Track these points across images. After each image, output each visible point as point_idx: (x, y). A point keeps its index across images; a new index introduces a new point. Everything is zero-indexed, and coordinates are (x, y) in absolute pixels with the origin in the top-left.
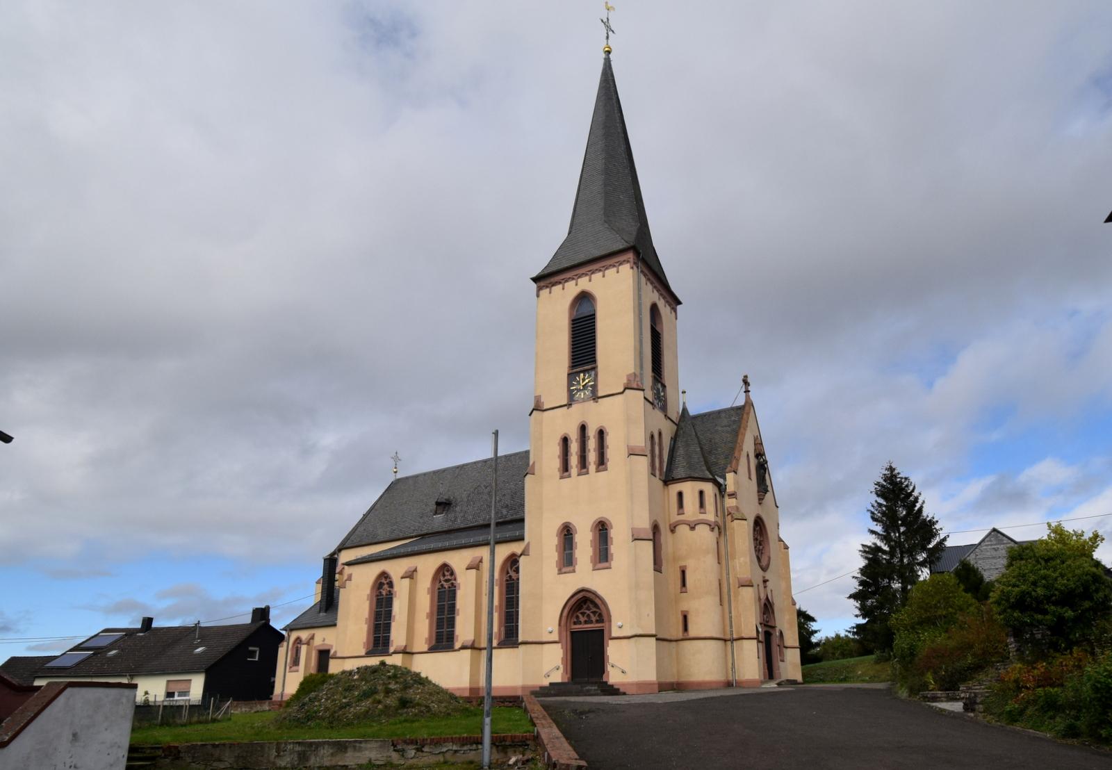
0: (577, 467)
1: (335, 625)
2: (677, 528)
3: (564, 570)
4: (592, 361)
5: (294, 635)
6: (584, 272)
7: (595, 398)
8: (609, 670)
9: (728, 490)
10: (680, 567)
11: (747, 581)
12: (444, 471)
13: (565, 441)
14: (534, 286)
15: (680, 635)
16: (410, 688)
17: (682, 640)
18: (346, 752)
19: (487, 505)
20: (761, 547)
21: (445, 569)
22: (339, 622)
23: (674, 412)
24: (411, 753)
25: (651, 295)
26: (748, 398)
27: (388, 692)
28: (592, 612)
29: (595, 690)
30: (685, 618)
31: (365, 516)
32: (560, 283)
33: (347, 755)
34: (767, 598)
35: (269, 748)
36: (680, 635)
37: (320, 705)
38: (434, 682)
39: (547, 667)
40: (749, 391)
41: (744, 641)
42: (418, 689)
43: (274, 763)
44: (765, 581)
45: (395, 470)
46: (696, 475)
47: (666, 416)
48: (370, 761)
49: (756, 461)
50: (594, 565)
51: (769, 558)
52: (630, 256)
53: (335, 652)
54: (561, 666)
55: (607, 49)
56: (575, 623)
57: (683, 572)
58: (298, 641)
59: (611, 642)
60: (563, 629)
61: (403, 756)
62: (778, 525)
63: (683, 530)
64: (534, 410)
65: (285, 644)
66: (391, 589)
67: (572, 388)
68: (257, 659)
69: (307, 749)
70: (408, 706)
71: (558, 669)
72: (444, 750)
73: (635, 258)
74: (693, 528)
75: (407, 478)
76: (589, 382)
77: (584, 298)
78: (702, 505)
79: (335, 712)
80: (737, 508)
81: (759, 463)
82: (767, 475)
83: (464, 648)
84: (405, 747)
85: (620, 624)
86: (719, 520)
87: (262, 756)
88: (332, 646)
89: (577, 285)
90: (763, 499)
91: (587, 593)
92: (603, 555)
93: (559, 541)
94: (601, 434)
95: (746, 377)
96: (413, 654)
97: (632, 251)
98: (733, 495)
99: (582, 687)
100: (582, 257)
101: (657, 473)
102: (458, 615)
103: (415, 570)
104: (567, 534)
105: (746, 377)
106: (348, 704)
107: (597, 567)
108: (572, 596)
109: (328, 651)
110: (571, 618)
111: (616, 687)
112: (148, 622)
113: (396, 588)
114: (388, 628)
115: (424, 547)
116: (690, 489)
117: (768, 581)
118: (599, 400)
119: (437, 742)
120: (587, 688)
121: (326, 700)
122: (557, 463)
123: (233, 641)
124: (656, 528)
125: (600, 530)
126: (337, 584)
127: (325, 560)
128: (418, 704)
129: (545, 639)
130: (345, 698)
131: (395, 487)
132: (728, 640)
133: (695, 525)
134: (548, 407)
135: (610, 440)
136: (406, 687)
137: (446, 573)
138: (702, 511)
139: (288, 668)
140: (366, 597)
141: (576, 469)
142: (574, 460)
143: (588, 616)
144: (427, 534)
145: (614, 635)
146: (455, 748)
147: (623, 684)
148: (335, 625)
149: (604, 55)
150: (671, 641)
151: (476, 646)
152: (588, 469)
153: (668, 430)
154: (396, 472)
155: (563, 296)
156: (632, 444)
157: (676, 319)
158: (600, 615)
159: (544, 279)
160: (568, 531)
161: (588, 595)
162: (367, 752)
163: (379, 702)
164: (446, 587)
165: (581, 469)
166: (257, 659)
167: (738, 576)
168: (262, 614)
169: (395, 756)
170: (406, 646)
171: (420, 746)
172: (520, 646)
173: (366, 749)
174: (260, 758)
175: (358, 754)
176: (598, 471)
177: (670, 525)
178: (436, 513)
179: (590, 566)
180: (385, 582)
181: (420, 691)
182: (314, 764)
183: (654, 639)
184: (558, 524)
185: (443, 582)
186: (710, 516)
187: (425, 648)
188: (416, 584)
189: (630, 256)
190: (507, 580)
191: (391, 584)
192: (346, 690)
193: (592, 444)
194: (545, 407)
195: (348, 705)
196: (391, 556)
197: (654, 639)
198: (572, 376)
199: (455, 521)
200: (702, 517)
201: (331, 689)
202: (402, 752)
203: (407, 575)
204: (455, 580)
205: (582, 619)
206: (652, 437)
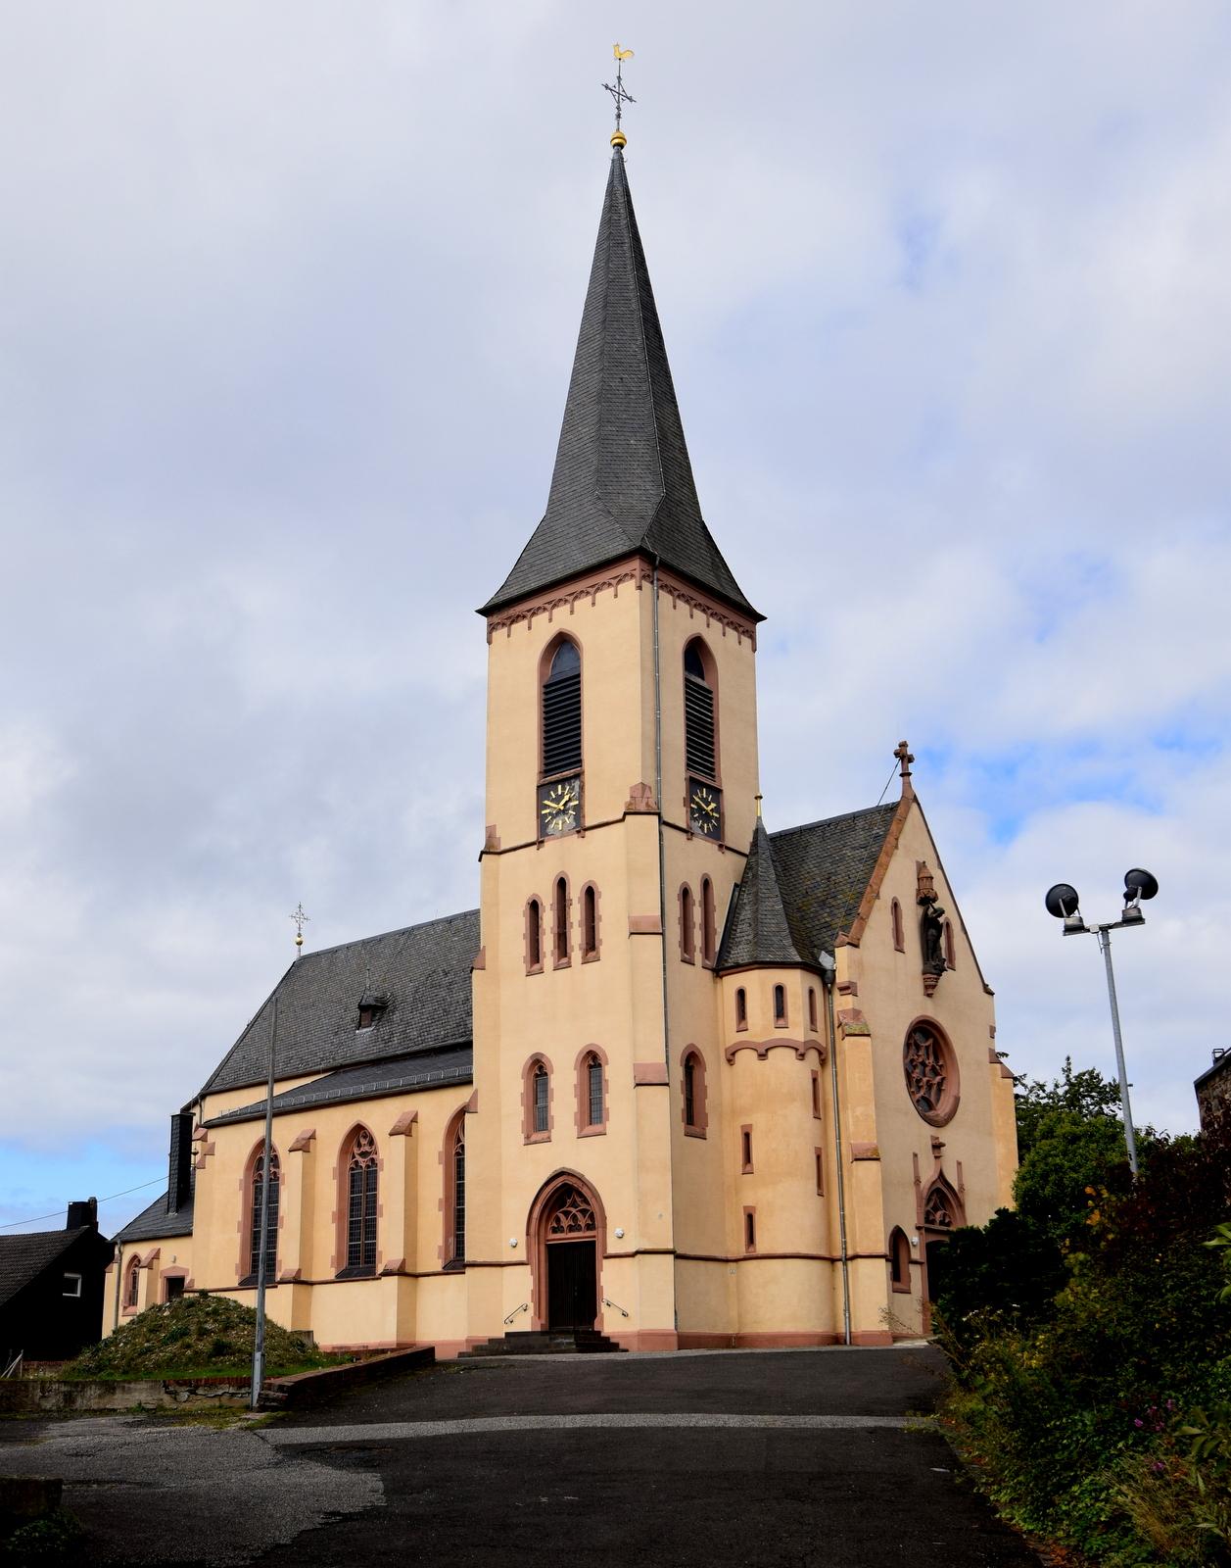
0: (553, 954)
1: (189, 1234)
2: (738, 1055)
3: (534, 1137)
4: (575, 763)
5: (129, 1251)
7: (581, 830)
9: (838, 980)
10: (742, 1127)
11: (867, 1150)
12: (380, 940)
13: (534, 907)
15: (742, 1252)
16: (233, 1328)
17: (745, 1259)
18: (113, 1394)
19: (445, 1010)
20: (938, 1078)
21: (359, 1134)
22: (196, 1230)
23: (739, 835)
24: (185, 1396)
25: (685, 621)
26: (907, 786)
27: (203, 1333)
28: (580, 1211)
29: (567, 1343)
30: (750, 1218)
31: (251, 1026)
32: (524, 617)
33: (116, 1397)
35: (33, 1387)
36: (739, 1248)
37: (117, 1351)
38: (279, 1325)
39: (509, 1306)
40: (910, 774)
41: (859, 1260)
42: (245, 1329)
43: (39, 1405)
44: (937, 1147)
45: (298, 939)
46: (770, 958)
47: (721, 846)
48: (140, 1404)
49: (921, 910)
50: (581, 1128)
51: (957, 1100)
52: (635, 565)
53: (192, 1281)
54: (531, 1306)
55: (617, 141)
56: (555, 1231)
57: (747, 1136)
58: (136, 1262)
59: (605, 1262)
60: (534, 1241)
61: (175, 1399)
62: (993, 1030)
63: (746, 1058)
64: (482, 853)
65: (115, 1266)
67: (543, 812)
68: (78, 1295)
69: (73, 1389)
70: (225, 1352)
72: (220, 1392)
73: (646, 566)
74: (763, 1056)
75: (318, 954)
76: (570, 800)
77: (563, 643)
78: (780, 1012)
79: (132, 1359)
80: (856, 1014)
81: (925, 916)
82: (943, 941)
83: (387, 1273)
84: (178, 1388)
85: (619, 1231)
86: (820, 1038)
87: (27, 1396)
88: (187, 1270)
89: (550, 620)
90: (934, 987)
91: (570, 1178)
92: (593, 1112)
93: (526, 1088)
94: (590, 893)
95: (903, 745)
96: (312, 1284)
98: (846, 989)
99: (551, 1339)
100: (560, 571)
101: (698, 957)
102: (382, 1216)
103: (313, 1137)
104: (538, 1071)
105: (903, 745)
106: (149, 1350)
107: (585, 1132)
108: (547, 1184)
109: (181, 1280)
110: (547, 1221)
111: (612, 1340)
113: (284, 1169)
114: (371, 1229)
115: (338, 1092)
116: (758, 984)
118: (587, 833)
119: (211, 1384)
120: (559, 1341)
121: (126, 1344)
122: (522, 948)
123: (39, 1260)
125: (537, 1076)
128: (240, 1351)
129: (505, 1260)
130: (148, 1341)
131: (302, 971)
132: (835, 1260)
133: (767, 1050)
134: (508, 847)
135: (603, 906)
136: (227, 1327)
137: (363, 1142)
139: (121, 1308)
142: (548, 942)
144: (342, 1067)
145: (611, 1251)
146: (232, 1390)
147: (625, 1336)
148: (189, 1234)
149: (611, 152)
150: (727, 1261)
151: (408, 1270)
152: (570, 958)
153: (724, 871)
154: (300, 943)
155: (534, 634)
156: (637, 913)
157: (754, 650)
158: (592, 1217)
159: (500, 611)
160: (541, 1068)
161: (571, 1181)
162: (137, 1394)
163: (188, 1346)
164: (364, 1165)
165: (531, 966)
166: (78, 1295)
167: (852, 1142)
168: (83, 1213)
169: (166, 1398)
170: (300, 1270)
171: (193, 1387)
172: (468, 1271)
173: (136, 1390)
174: (25, 1399)
175: (127, 1396)
177: (726, 1050)
178: (359, 1026)
179: (574, 1130)
181: (246, 1332)
182: (81, 1406)
183: (672, 1256)
184: (523, 1058)
185: (358, 1158)
186: (797, 1028)
187: (331, 1274)
188: (315, 1160)
190: (352, 1169)
191: (275, 1160)
192: (151, 1331)
193: (576, 913)
194: (503, 847)
195: (150, 1351)
196: (307, 1105)
197: (672, 1256)
198: (543, 790)
199: (390, 1040)
200: (743, 1037)
201: (133, 1329)
202: (174, 1395)
203: (299, 1146)
205: (565, 1222)
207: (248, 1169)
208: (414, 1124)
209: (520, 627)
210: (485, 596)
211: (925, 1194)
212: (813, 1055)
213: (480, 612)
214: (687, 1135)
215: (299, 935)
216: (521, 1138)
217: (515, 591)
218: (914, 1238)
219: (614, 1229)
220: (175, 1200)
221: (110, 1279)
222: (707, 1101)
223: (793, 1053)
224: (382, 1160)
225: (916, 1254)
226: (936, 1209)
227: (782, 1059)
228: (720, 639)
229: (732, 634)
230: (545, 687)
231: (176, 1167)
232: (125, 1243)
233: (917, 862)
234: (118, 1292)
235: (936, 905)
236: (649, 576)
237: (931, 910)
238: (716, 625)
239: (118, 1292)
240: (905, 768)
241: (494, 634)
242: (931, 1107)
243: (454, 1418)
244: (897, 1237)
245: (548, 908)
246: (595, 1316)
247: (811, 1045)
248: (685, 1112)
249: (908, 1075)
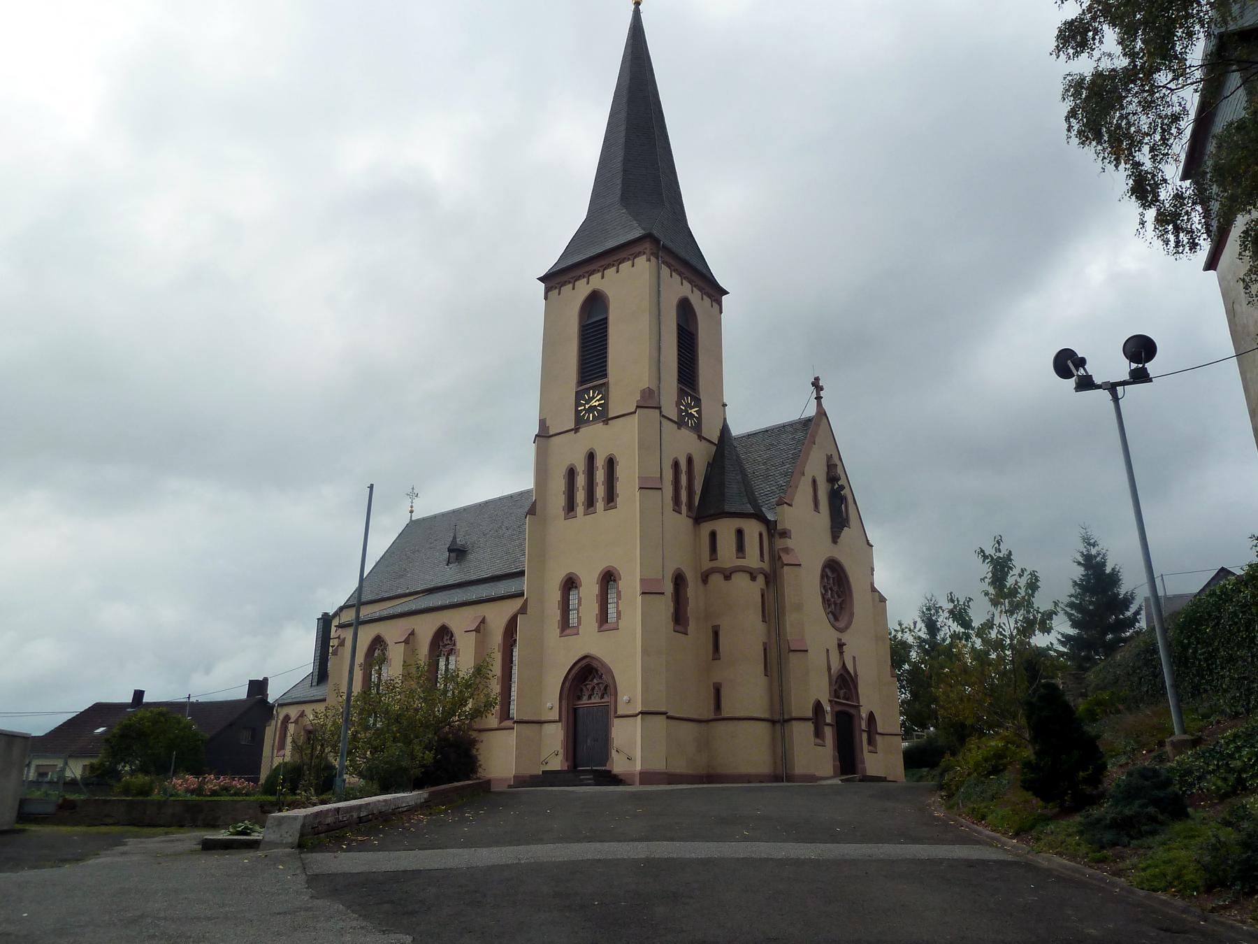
5: (283, 713)
6: (581, 274)
9: (778, 528)
13: (571, 473)
15: (712, 716)
25: (677, 288)
26: (819, 404)
44: (841, 646)
49: (829, 486)
57: (716, 634)
59: (616, 722)
63: (716, 579)
65: (273, 723)
67: (579, 409)
78: (740, 548)
94: (611, 463)
95: (817, 379)
97: (648, 240)
101: (684, 508)
105: (817, 379)
112: (139, 694)
124: (679, 580)
133: (731, 574)
135: (620, 471)
138: (740, 555)
139: (276, 751)
142: (580, 496)
145: (620, 712)
157: (721, 312)
165: (568, 513)
168: (258, 687)
186: (753, 559)
189: (647, 246)
193: (600, 476)
194: (551, 433)
197: (665, 716)
198: (579, 396)
204: (454, 645)
211: (834, 678)
212: (761, 579)
213: (541, 279)
214: (675, 631)
215: (412, 507)
216: (558, 631)
218: (828, 708)
219: (623, 697)
220: (317, 677)
222: (688, 608)
223: (748, 575)
225: (829, 719)
226: (841, 688)
227: (741, 580)
228: (700, 303)
229: (707, 300)
230: (583, 326)
231: (318, 654)
232: (281, 705)
233: (827, 455)
234: (275, 735)
235: (840, 483)
236: (655, 254)
237: (836, 486)
238: (697, 293)
239: (275, 735)
240: (818, 393)
241: (549, 293)
242: (836, 619)
243: (511, 843)
244: (818, 707)
246: (608, 759)
247: (762, 571)
248: (674, 616)
249: (823, 596)
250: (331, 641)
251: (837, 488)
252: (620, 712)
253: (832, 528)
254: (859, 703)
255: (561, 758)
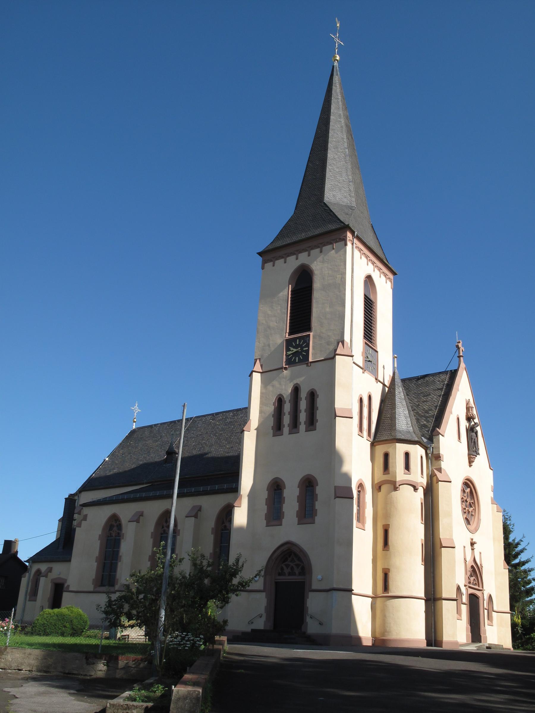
0: (305, 423)
5: (36, 567)
8: (307, 621)
14: (260, 259)
34: (475, 560)
44: (472, 544)
47: (376, 379)
53: (68, 586)
56: (280, 574)
59: (311, 594)
65: (27, 574)
66: (120, 531)
71: (261, 617)
78: (407, 467)
85: (319, 577)
101: (365, 433)
117: (475, 543)
126: (75, 523)
127: (66, 499)
140: (97, 537)
141: (305, 426)
142: (287, 420)
143: (292, 568)
145: (314, 587)
158: (303, 568)
176: (290, 433)
179: (296, 520)
180: (115, 524)
191: (120, 527)
193: (303, 405)
206: (361, 400)
207: (104, 529)
208: (199, 512)
209: (280, 263)
210: (264, 244)
213: (260, 254)
217: (279, 243)
218: (463, 589)
221: (24, 581)
224: (179, 530)
237: (473, 423)
238: (377, 272)
245: (287, 402)
250: (75, 515)
251: (388, 391)
252: (314, 587)
253: (469, 455)
254: (483, 588)
255: (66, 584)
